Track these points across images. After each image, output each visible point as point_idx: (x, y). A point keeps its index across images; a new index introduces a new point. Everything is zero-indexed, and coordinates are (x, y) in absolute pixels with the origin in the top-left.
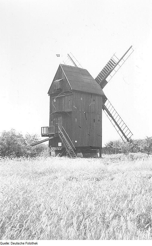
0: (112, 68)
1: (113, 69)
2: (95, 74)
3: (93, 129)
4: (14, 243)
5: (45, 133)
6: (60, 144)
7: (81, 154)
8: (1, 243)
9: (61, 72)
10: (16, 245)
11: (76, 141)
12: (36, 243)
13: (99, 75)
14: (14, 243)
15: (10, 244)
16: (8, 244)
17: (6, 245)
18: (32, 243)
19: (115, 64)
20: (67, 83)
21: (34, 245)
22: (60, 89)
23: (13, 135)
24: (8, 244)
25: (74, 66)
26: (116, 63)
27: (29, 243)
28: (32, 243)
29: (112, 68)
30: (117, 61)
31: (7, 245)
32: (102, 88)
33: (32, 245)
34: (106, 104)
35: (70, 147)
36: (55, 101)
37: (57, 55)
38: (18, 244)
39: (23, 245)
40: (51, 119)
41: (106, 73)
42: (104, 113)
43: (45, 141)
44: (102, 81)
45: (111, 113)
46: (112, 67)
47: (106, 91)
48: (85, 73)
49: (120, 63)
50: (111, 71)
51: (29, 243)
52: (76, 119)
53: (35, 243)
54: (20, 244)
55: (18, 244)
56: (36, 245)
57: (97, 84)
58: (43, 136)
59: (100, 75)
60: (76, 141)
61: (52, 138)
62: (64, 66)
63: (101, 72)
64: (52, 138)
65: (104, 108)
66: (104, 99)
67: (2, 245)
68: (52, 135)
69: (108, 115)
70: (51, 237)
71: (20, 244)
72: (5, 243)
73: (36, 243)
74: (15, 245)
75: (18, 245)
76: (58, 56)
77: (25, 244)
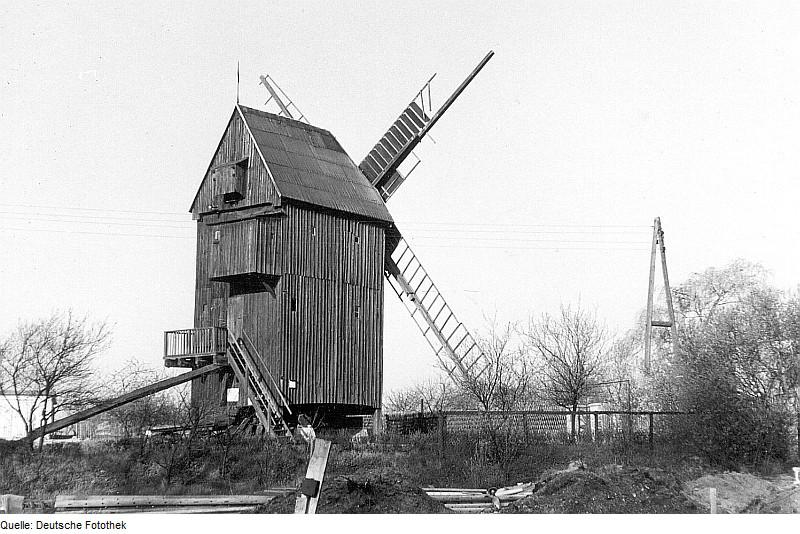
0: (420, 130)
2: (358, 150)
4: (46, 525)
5: (180, 351)
8: (4, 525)
13: (372, 152)
15: (34, 526)
16: (26, 526)
19: (426, 118)
20: (261, 173)
23: (90, 458)
24: (26, 526)
25: (273, 109)
27: (98, 525)
28: (109, 525)
29: (420, 130)
30: (431, 115)
31: (24, 531)
33: (106, 531)
34: (395, 256)
35: (272, 406)
38: (61, 526)
40: (200, 304)
42: (390, 288)
44: (385, 170)
46: (422, 126)
47: (399, 207)
50: (418, 140)
51: (98, 525)
53: (118, 524)
54: (68, 526)
55: (61, 526)
57: (369, 184)
58: (171, 362)
60: (292, 384)
62: (250, 112)
63: (382, 140)
65: (392, 269)
66: (393, 236)
67: (8, 531)
71: (68, 526)
72: (17, 525)
74: (49, 531)
75: (59, 531)
77: (84, 525)
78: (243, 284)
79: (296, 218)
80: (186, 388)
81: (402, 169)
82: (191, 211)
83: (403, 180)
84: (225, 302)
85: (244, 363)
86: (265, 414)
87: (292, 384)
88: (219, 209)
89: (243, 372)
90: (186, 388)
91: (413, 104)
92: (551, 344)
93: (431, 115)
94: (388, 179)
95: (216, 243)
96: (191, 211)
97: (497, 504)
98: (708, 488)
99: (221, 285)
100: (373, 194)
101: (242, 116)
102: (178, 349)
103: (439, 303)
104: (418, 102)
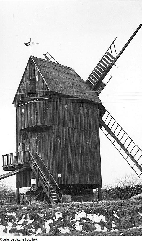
0: (113, 60)
1: (113, 64)
2: (85, 73)
3: (87, 154)
4: (13, 240)
6: (33, 182)
7: (69, 196)
8: (1, 239)
9: (33, 68)
10: (16, 241)
11: (59, 175)
14: (13, 240)
15: (10, 240)
16: (8, 240)
17: (6, 241)
18: (32, 239)
19: (113, 58)
20: (41, 82)
21: (34, 241)
22: (31, 92)
24: (8, 240)
27: (29, 239)
28: (32, 239)
30: (115, 56)
31: (7, 241)
32: (98, 94)
33: (31, 241)
34: (104, 119)
35: (49, 185)
36: (23, 111)
38: (18, 240)
39: (23, 241)
41: (102, 71)
42: (102, 133)
44: (97, 84)
47: (104, 97)
50: (110, 67)
51: (29, 239)
53: (35, 239)
54: (20, 240)
55: (18, 240)
56: (36, 241)
59: (93, 75)
61: (20, 170)
62: (36, 59)
64: (20, 170)
65: (102, 124)
66: (102, 110)
67: (2, 241)
68: (20, 166)
69: (109, 136)
71: (20, 240)
72: (5, 239)
74: (14, 241)
75: (17, 241)
76: (28, 44)
77: (25, 240)
78: (35, 130)
79: (56, 101)
81: (105, 81)
82: (13, 103)
83: (105, 85)
84: (29, 141)
85: (37, 167)
86: (47, 189)
87: (59, 175)
88: (24, 99)
89: (36, 170)
91: (107, 52)
93: (115, 56)
95: (23, 114)
96: (13, 103)
97: (79, 228)
99: (24, 132)
100: (92, 93)
101: (32, 61)
102: (9, 162)
103: (129, 140)
104: (109, 51)
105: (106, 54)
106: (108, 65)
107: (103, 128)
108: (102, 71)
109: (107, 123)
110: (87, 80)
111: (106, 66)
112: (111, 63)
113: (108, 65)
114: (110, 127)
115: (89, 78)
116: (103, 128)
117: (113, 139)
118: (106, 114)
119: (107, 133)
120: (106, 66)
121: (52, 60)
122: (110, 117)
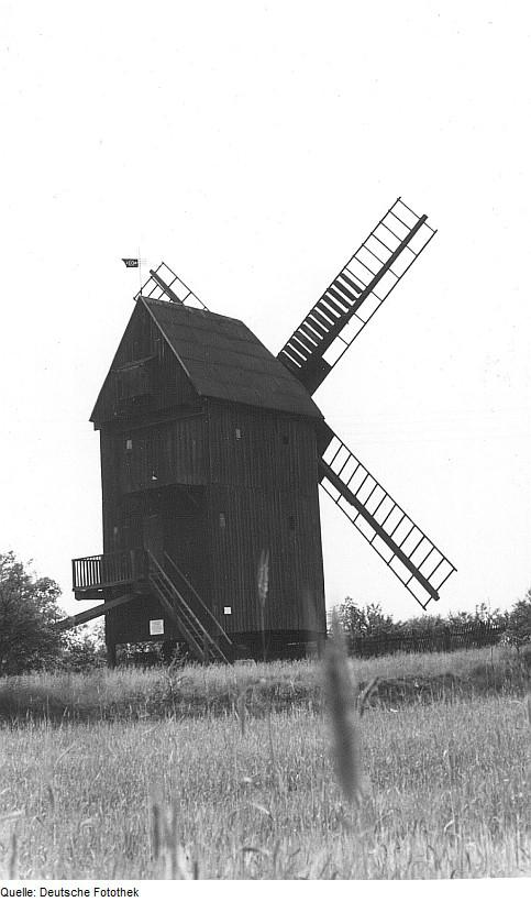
0: (352, 303)
2: (274, 339)
4: (50, 893)
8: (4, 892)
12: (133, 893)
14: (50, 893)
15: (37, 893)
16: (29, 893)
18: (119, 892)
24: (29, 893)
25: (202, 307)
26: (363, 288)
27: (107, 893)
28: (119, 892)
30: (368, 279)
34: (327, 457)
37: (124, 260)
38: (67, 893)
41: (347, 305)
42: (326, 492)
43: (83, 618)
44: (307, 363)
45: (353, 488)
47: (323, 397)
48: (235, 334)
49: (381, 288)
51: (107, 893)
52: (222, 515)
53: (130, 892)
54: (74, 893)
55: (67, 893)
61: (124, 599)
64: (124, 599)
65: (326, 471)
67: (9, 899)
68: (123, 590)
69: (343, 501)
70: (344, 878)
71: (74, 893)
72: (19, 891)
73: (133, 893)
77: (92, 893)
80: (100, 621)
82: (91, 420)
88: (118, 413)
90: (100, 621)
92: (392, 846)
94: (317, 371)
96: (91, 420)
98: (477, 847)
101: (143, 307)
105: (333, 287)
106: (338, 316)
107: (325, 481)
108: (347, 305)
109: (336, 468)
110: (281, 354)
111: (336, 311)
112: (346, 310)
113: (338, 316)
114: (344, 478)
115: (286, 347)
116: (325, 481)
117: (353, 511)
118: (334, 445)
119: (336, 493)
120: (336, 311)
121: (190, 303)
122: (344, 454)
